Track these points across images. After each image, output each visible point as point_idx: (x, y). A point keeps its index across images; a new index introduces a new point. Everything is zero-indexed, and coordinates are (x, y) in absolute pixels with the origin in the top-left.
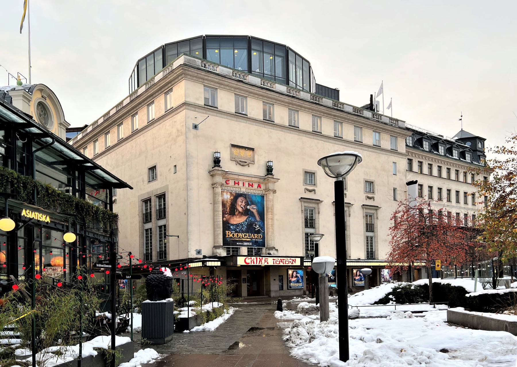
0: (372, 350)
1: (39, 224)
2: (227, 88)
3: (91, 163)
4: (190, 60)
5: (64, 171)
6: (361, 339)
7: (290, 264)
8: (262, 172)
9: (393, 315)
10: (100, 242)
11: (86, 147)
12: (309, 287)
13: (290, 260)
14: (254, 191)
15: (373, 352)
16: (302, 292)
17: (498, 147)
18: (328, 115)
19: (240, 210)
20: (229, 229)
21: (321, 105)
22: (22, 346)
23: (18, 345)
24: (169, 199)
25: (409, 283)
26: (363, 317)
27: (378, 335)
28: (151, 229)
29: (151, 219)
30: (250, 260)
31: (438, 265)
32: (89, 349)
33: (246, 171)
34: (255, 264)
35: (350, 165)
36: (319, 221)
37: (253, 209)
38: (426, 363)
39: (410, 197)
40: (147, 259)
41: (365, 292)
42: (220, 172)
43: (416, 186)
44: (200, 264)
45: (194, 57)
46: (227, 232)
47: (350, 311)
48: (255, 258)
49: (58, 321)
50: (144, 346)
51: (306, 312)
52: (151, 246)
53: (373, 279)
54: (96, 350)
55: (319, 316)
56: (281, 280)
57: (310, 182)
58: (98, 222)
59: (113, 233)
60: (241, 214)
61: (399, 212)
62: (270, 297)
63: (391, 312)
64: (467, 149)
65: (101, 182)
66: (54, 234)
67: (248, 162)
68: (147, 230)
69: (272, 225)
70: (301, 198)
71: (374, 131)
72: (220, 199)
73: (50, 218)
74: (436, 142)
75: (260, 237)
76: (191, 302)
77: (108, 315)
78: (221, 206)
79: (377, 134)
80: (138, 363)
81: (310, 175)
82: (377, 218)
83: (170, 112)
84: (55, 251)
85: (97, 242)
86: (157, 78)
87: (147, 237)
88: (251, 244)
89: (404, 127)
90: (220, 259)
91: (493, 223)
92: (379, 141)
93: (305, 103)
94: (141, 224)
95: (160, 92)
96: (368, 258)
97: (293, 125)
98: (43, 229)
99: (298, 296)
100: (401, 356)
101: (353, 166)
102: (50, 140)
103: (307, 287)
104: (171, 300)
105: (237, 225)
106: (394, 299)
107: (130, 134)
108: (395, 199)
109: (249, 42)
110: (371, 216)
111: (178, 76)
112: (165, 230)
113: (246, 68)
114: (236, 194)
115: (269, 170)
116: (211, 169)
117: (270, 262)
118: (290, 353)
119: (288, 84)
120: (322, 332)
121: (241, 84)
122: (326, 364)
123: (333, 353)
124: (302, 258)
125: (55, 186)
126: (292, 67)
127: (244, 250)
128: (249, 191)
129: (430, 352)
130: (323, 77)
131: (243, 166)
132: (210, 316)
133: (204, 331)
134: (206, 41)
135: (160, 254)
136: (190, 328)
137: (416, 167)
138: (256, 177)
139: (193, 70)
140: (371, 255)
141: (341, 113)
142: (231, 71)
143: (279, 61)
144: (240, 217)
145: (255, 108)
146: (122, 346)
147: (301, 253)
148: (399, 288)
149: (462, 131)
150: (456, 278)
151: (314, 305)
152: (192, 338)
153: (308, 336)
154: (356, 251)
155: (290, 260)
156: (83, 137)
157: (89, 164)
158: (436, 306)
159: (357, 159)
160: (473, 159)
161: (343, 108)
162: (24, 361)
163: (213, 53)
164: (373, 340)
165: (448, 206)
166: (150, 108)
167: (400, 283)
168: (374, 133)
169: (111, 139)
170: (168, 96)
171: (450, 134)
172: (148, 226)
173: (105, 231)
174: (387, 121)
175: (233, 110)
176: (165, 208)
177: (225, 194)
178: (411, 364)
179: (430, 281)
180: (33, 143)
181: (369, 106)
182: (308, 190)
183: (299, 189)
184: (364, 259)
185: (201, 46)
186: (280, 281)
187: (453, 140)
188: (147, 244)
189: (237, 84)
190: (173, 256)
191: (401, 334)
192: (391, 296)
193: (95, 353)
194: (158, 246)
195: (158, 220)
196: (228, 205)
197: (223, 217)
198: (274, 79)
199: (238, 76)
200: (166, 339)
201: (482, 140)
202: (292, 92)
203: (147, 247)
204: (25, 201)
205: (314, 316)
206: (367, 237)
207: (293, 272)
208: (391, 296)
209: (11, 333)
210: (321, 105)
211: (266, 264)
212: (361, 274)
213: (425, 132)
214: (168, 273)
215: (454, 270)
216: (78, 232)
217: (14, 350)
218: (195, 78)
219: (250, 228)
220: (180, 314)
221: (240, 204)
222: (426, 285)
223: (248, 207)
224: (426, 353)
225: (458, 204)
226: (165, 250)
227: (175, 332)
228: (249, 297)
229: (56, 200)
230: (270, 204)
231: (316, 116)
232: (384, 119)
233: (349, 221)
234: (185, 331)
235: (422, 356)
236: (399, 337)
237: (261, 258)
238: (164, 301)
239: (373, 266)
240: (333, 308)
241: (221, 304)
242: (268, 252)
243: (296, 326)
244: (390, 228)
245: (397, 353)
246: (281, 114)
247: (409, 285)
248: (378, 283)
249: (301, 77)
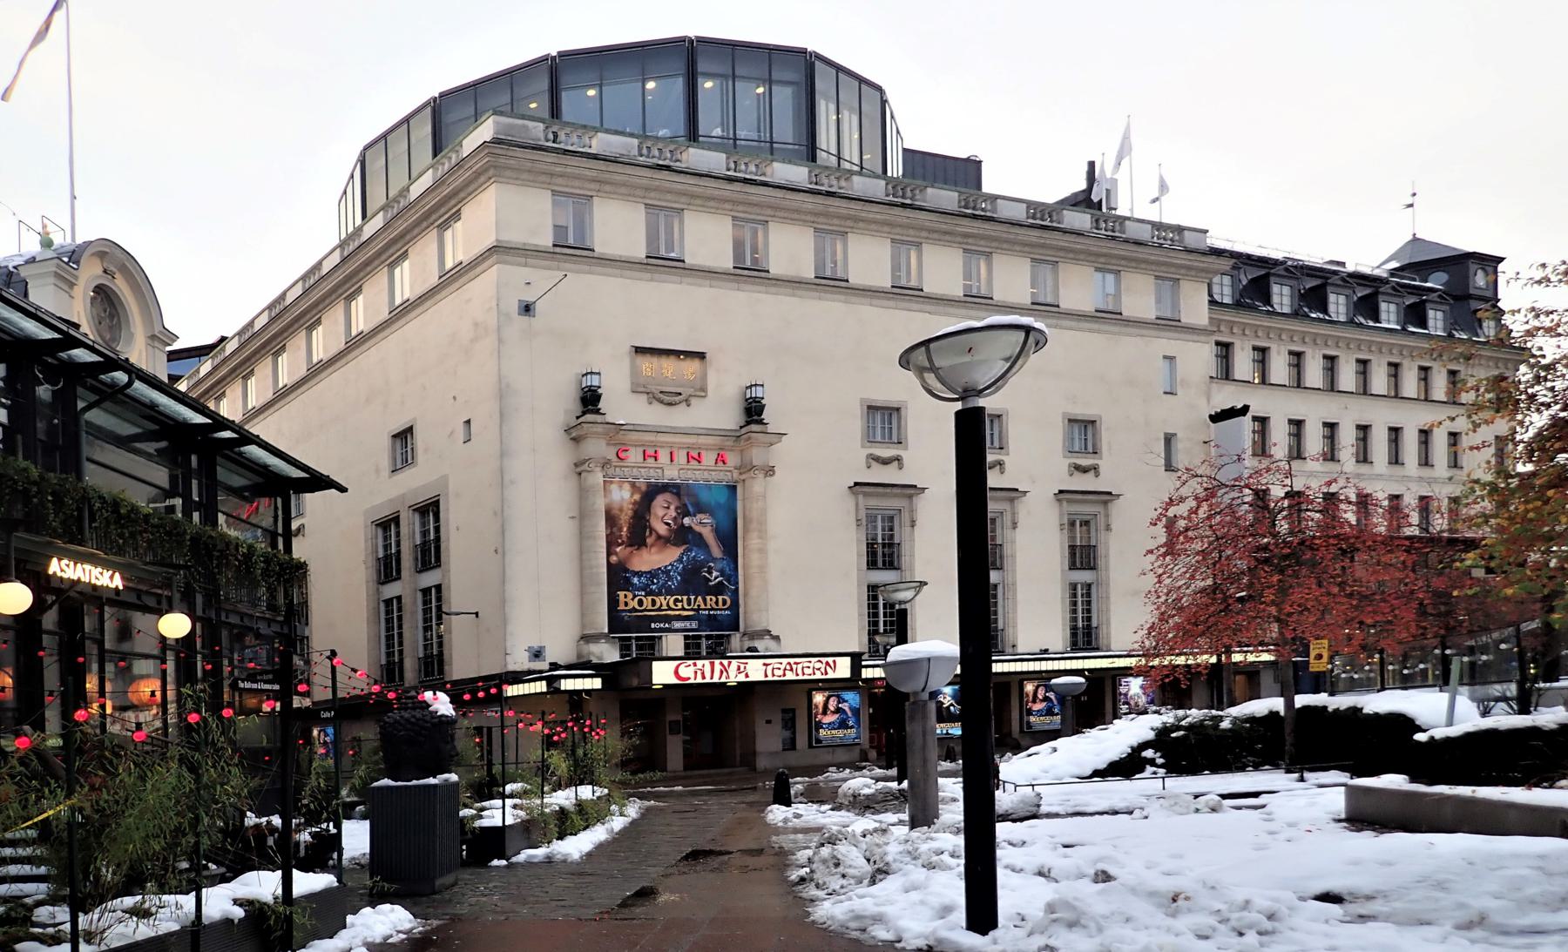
0: (1076, 899)
1: (96, 596)
2: (623, 190)
3: (233, 431)
4: (512, 126)
5: (161, 457)
6: (1040, 874)
7: (818, 676)
8: (731, 418)
9: (1153, 808)
10: (258, 636)
11: (223, 394)
12: (880, 740)
13: (818, 665)
14: (706, 474)
15: (1076, 903)
16: (856, 753)
17: (1544, 266)
18: (944, 237)
19: (662, 530)
20: (627, 585)
21: (921, 209)
22: (52, 900)
23: (41, 897)
24: (454, 517)
25: (1214, 712)
26: (1049, 816)
27: (1096, 862)
28: (399, 598)
29: (399, 571)
30: (692, 668)
31: (1319, 656)
32: (220, 902)
33: (679, 417)
34: (708, 680)
35: (1007, 360)
36: (912, 547)
37: (703, 524)
38: (1260, 933)
39: (1221, 451)
40: (391, 679)
41: (1061, 743)
42: (599, 429)
43: (1246, 422)
44: (541, 687)
45: (523, 117)
46: (621, 594)
47: (1004, 799)
48: (707, 662)
49: (136, 833)
50: (375, 899)
51: (863, 805)
52: (401, 644)
53: (1092, 704)
54: (241, 905)
55: (905, 817)
56: (790, 723)
57: (883, 436)
58: (255, 585)
59: (297, 613)
61: (1182, 500)
63: (1148, 797)
64: (1434, 296)
65: (260, 480)
66: (140, 620)
67: (686, 392)
68: (388, 602)
69: (763, 568)
70: (1061, 492)
71: (1098, 270)
72: (600, 504)
73: (123, 578)
74: (1315, 285)
75: (724, 602)
76: (509, 788)
77: (277, 821)
78: (603, 523)
79: (1110, 278)
80: (358, 941)
81: (884, 419)
82: (1108, 528)
83: (452, 278)
84: (141, 667)
85: (249, 639)
86: (417, 190)
87: (389, 621)
88: (694, 625)
89: (1202, 246)
90: (599, 669)
91: (1522, 508)
92: (1117, 296)
93: (868, 207)
94: (373, 585)
95: (425, 224)
96: (1075, 646)
97: (828, 274)
98: (106, 608)
99: (841, 766)
100: (1173, 915)
101: (1014, 361)
102: (121, 377)
103: (871, 740)
104: (454, 777)
105: (652, 574)
106: (1160, 761)
107: (342, 346)
108: (1169, 467)
109: (688, 57)
110: (1086, 523)
111: (478, 174)
112: (439, 599)
113: (680, 127)
114: (649, 485)
115: (753, 411)
116: (574, 422)
117: (756, 671)
118: (809, 914)
119: (814, 159)
120: (914, 856)
121: (665, 175)
122: (921, 943)
123: (946, 910)
124: (856, 658)
125: (140, 498)
126: (825, 112)
127: (674, 643)
128: (690, 474)
129: (1274, 900)
130: (923, 125)
131: (670, 404)
132: (566, 824)
133: (549, 860)
134: (558, 71)
135: (426, 664)
136: (509, 853)
137: (1243, 364)
138: (709, 433)
139: (519, 152)
140: (1084, 637)
141: (987, 225)
142: (635, 142)
143: (785, 98)
144: (660, 551)
145: (707, 237)
146: (311, 897)
147: (856, 641)
148: (1179, 728)
149: (1415, 240)
150: (1383, 689)
151: (894, 785)
152: (513, 880)
153: (869, 868)
154: (1034, 628)
155: (818, 665)
156: (215, 369)
157: (227, 434)
158: (1306, 775)
159: (1031, 340)
160: (1452, 324)
161: (994, 211)
162: (50, 930)
163: (582, 98)
164: (1082, 876)
165: (1358, 476)
166: (397, 271)
167: (1181, 713)
168: (1099, 275)
169: (289, 367)
170: (448, 234)
171: (1370, 251)
172: (391, 590)
173: (272, 607)
174: (1145, 233)
175: (640, 253)
176: (438, 539)
177: (614, 487)
178: (1207, 938)
179: (1289, 704)
180: (80, 390)
181: (1081, 198)
182: (878, 460)
183: (851, 459)
184: (1060, 648)
185: (544, 84)
186: (785, 727)
187: (1381, 273)
188: (389, 638)
189: (657, 177)
190: (461, 666)
191: (1181, 857)
192: (1149, 753)
193: (239, 913)
194: (421, 643)
195: (420, 572)
196: (625, 519)
197: (609, 554)
198: (771, 149)
199: (656, 153)
200: (439, 882)
201: (1491, 263)
202: (825, 181)
203: (388, 646)
204: (59, 537)
205: (890, 817)
206: (1074, 587)
207: (828, 698)
208: (1149, 753)
209: (26, 869)
210: (921, 209)
211: (742, 678)
212: (1051, 695)
213: (1277, 255)
214: (442, 704)
215: (1376, 667)
216: (199, 612)
217: (31, 909)
218: (525, 176)
219: (692, 580)
220: (481, 817)
221: (662, 514)
222: (1273, 715)
223: (687, 521)
224: (1261, 902)
225: (1397, 468)
226: (441, 654)
227: (465, 864)
228: (689, 773)
229: (141, 533)
230: (755, 508)
231: (903, 242)
232: (1132, 231)
233: (1013, 542)
234: (496, 862)
235: (1245, 914)
236: (1170, 865)
237: (725, 662)
238: (431, 781)
239: (1090, 670)
240: (951, 788)
241: (599, 792)
242: (747, 644)
243: (832, 841)
244: (1151, 552)
245: (1160, 906)
246: (790, 248)
247: (1213, 718)
248: (1109, 715)
249: (856, 136)
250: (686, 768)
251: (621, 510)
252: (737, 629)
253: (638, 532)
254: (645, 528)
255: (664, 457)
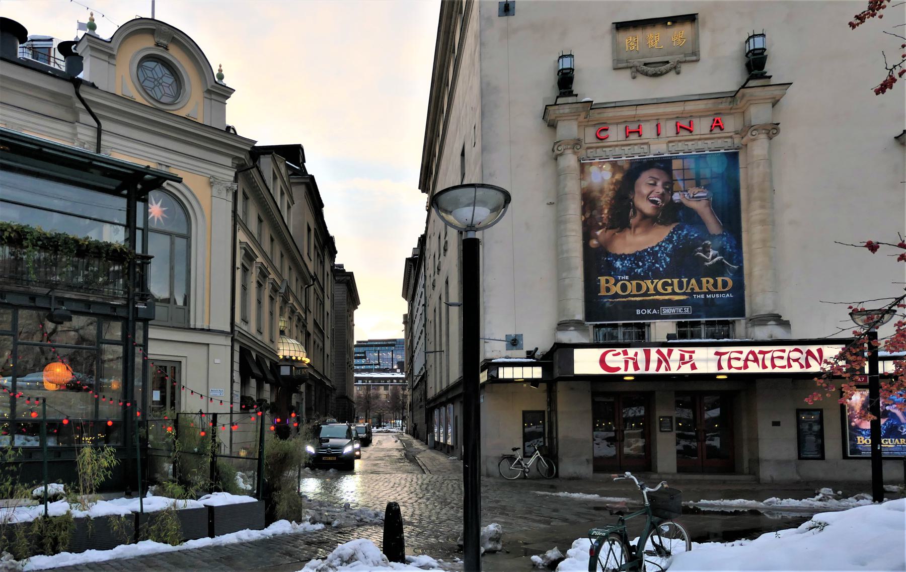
7: (796, 368)
19: (647, 208)
20: (610, 270)
30: (622, 356)
37: (697, 201)
46: (603, 279)
60: (650, 221)
62: (758, 481)
75: (725, 284)
88: (687, 310)
105: (637, 257)
114: (632, 162)
115: (755, 63)
128: (680, 146)
131: (655, 75)
144: (647, 230)
177: (594, 169)
196: (605, 201)
211: (686, 370)
219: (684, 261)
221: (647, 193)
250: (681, 469)
251: (602, 191)
252: (742, 314)
253: (622, 212)
254: (628, 208)
255: (648, 130)
